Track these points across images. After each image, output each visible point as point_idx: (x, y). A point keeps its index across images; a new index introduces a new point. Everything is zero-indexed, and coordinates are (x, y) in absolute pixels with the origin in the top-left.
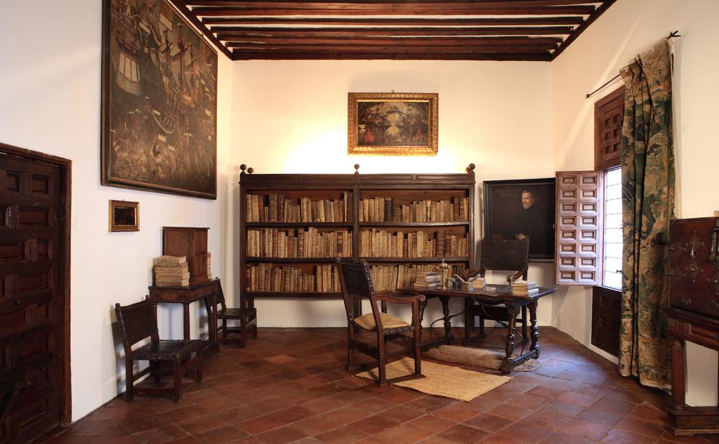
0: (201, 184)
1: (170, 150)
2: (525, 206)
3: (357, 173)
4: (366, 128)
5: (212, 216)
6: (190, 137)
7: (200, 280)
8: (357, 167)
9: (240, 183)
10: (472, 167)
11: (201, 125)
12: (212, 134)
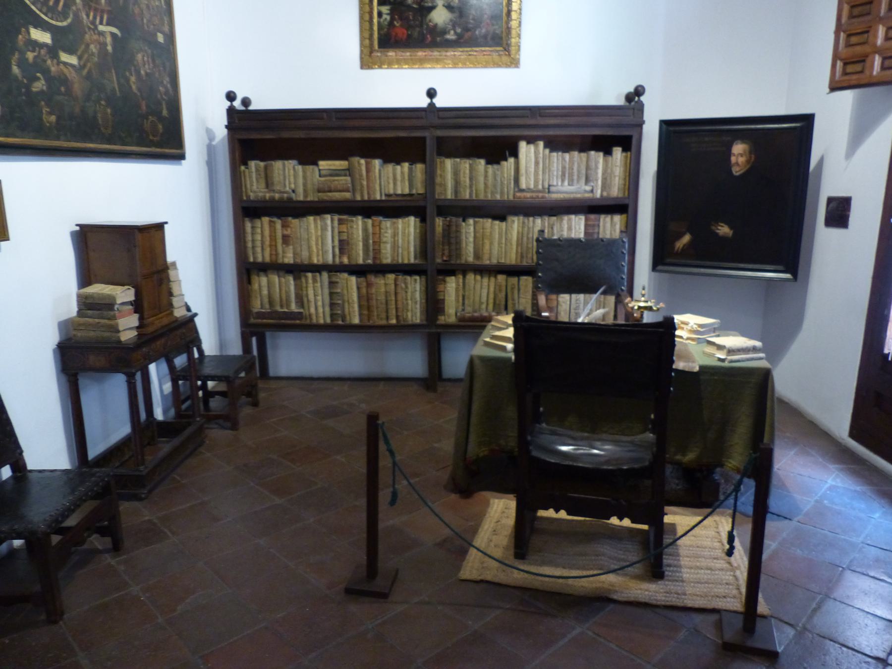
0: (152, 132)
1: (65, 64)
2: (737, 171)
3: (432, 105)
4: (392, 13)
5: (170, 196)
6: (113, 35)
7: (157, 323)
8: (431, 93)
9: (227, 127)
10: (639, 91)
11: (137, 11)
12: (166, 29)
